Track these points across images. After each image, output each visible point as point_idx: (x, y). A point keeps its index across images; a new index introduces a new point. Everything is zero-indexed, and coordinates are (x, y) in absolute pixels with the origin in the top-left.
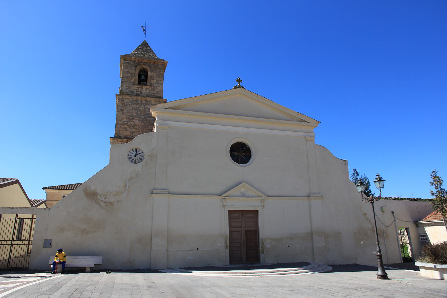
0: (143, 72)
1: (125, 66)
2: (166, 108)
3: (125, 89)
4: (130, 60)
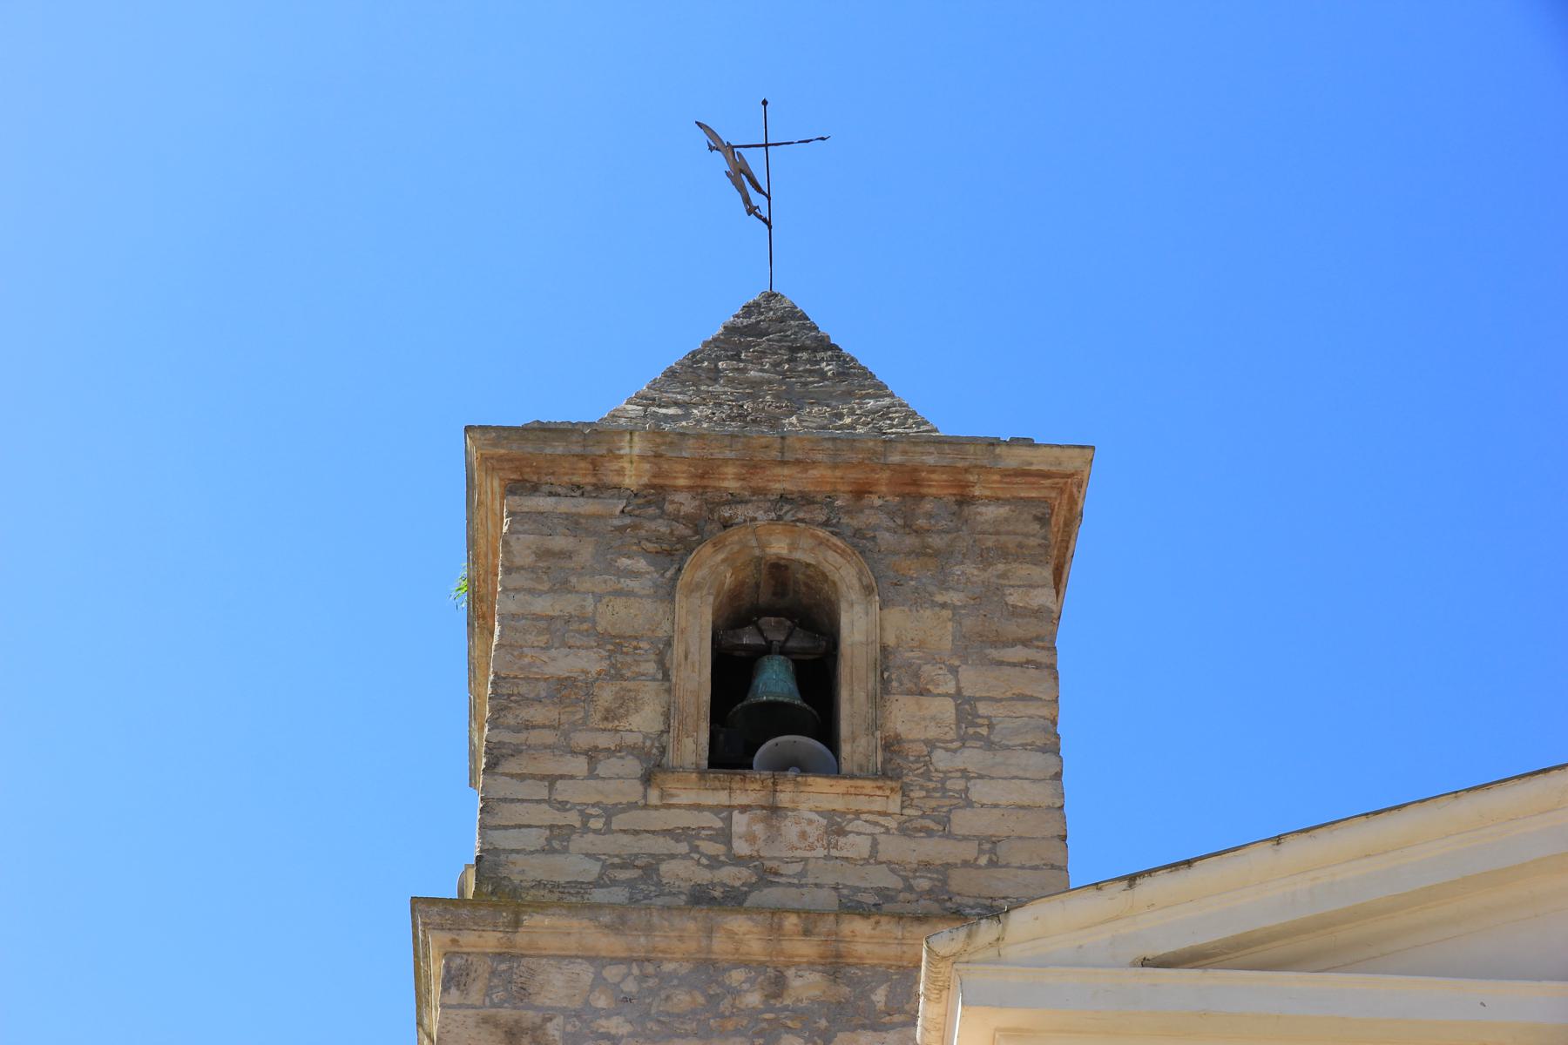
0: (768, 622)
1: (524, 558)
2: (1150, 953)
3: (535, 839)
4: (596, 487)
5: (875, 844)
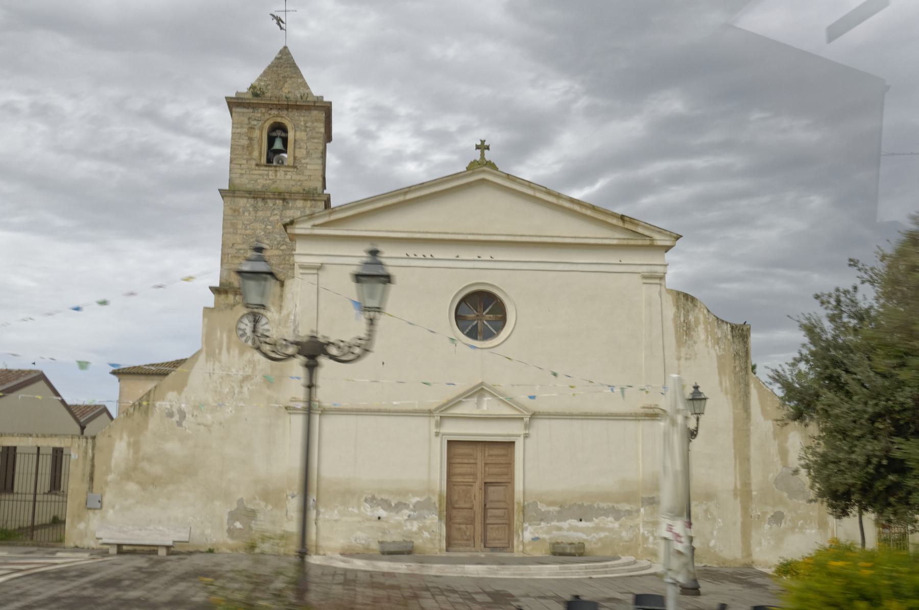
5: (291, 177)
